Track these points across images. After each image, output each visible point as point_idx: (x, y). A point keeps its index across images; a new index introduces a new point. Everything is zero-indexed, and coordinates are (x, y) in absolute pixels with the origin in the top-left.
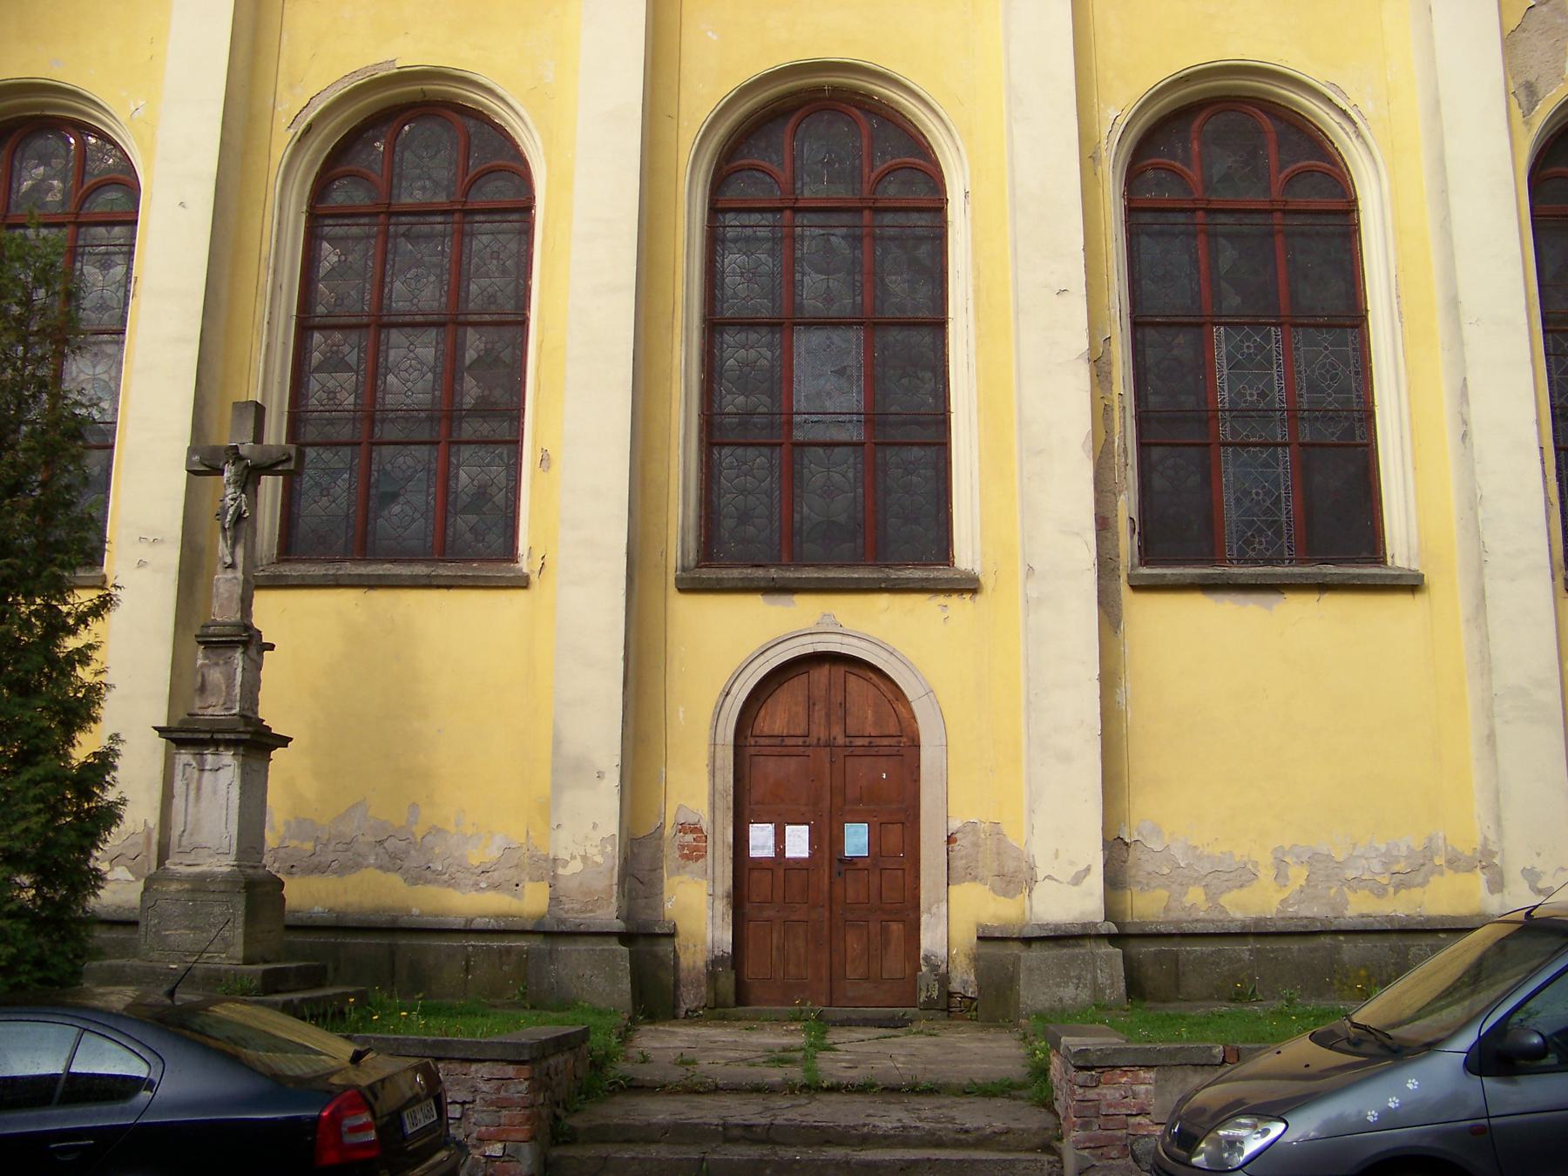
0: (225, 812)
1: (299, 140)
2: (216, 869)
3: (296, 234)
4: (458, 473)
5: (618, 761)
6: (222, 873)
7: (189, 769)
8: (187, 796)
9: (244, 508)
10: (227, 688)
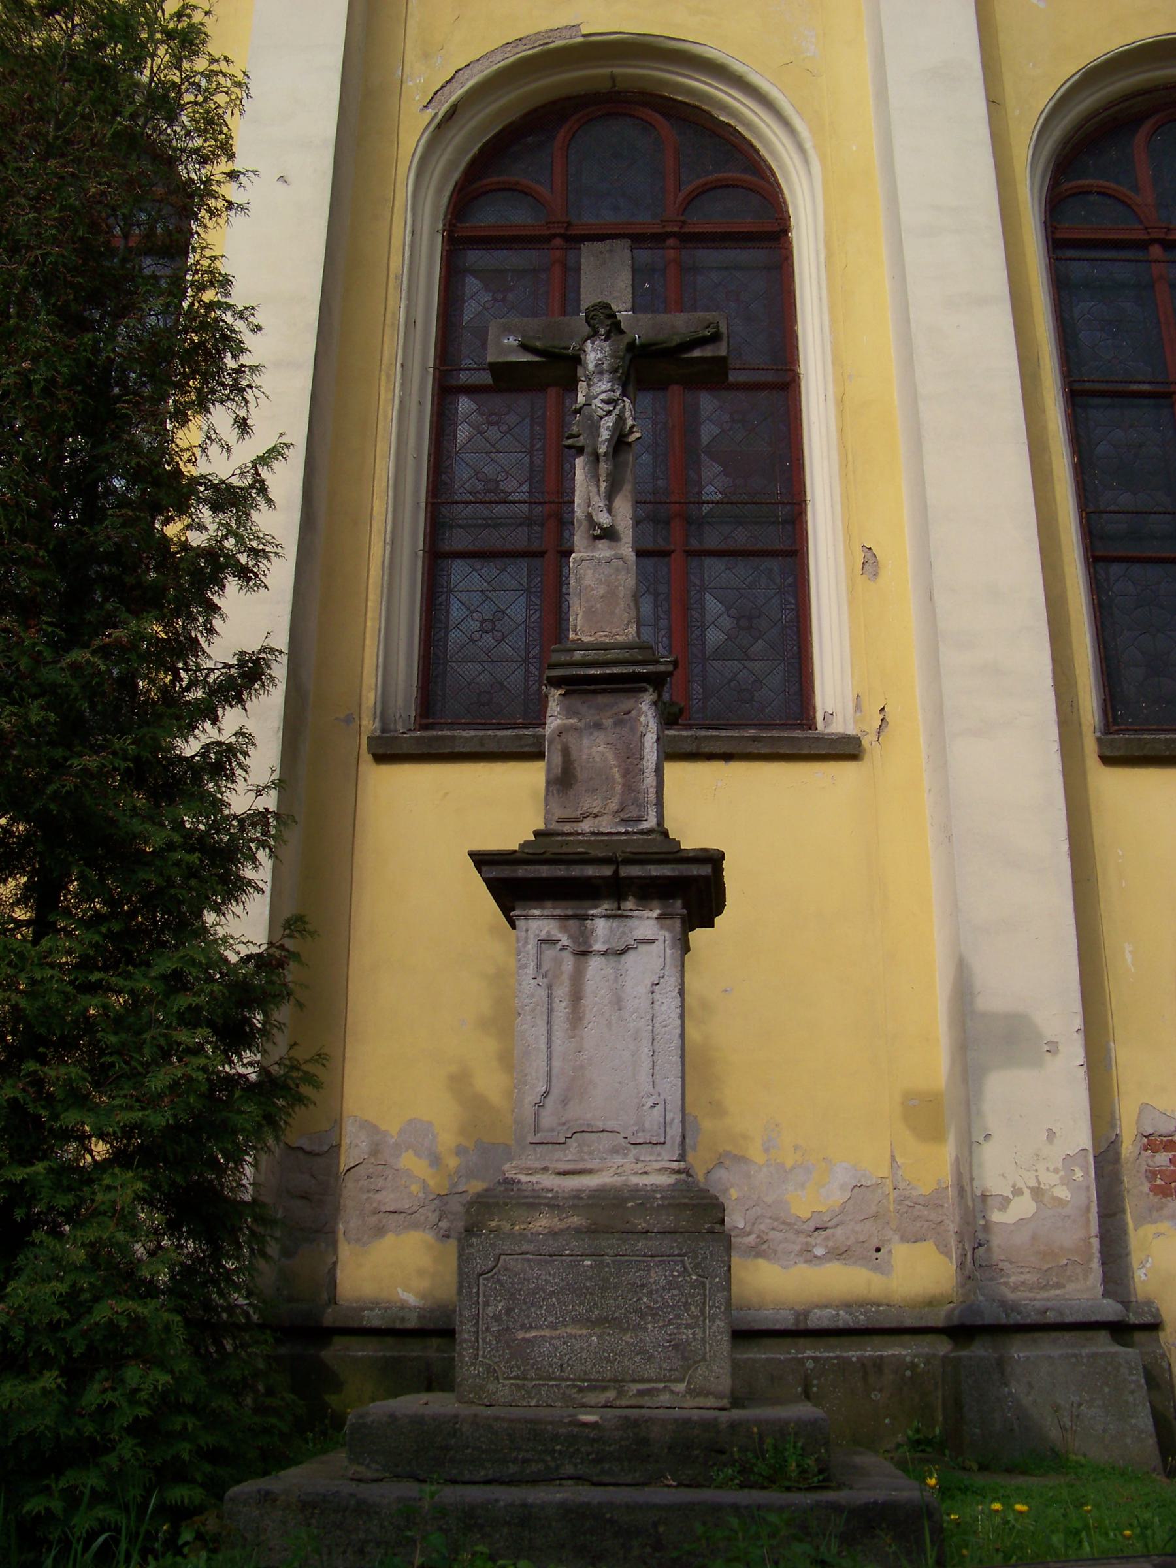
0: (646, 1050)
1: (439, 126)
2: (635, 1180)
3: (431, 256)
4: (703, 598)
5: (1078, 1022)
6: (656, 1188)
7: (549, 953)
8: (550, 1011)
9: (630, 422)
10: (624, 776)
